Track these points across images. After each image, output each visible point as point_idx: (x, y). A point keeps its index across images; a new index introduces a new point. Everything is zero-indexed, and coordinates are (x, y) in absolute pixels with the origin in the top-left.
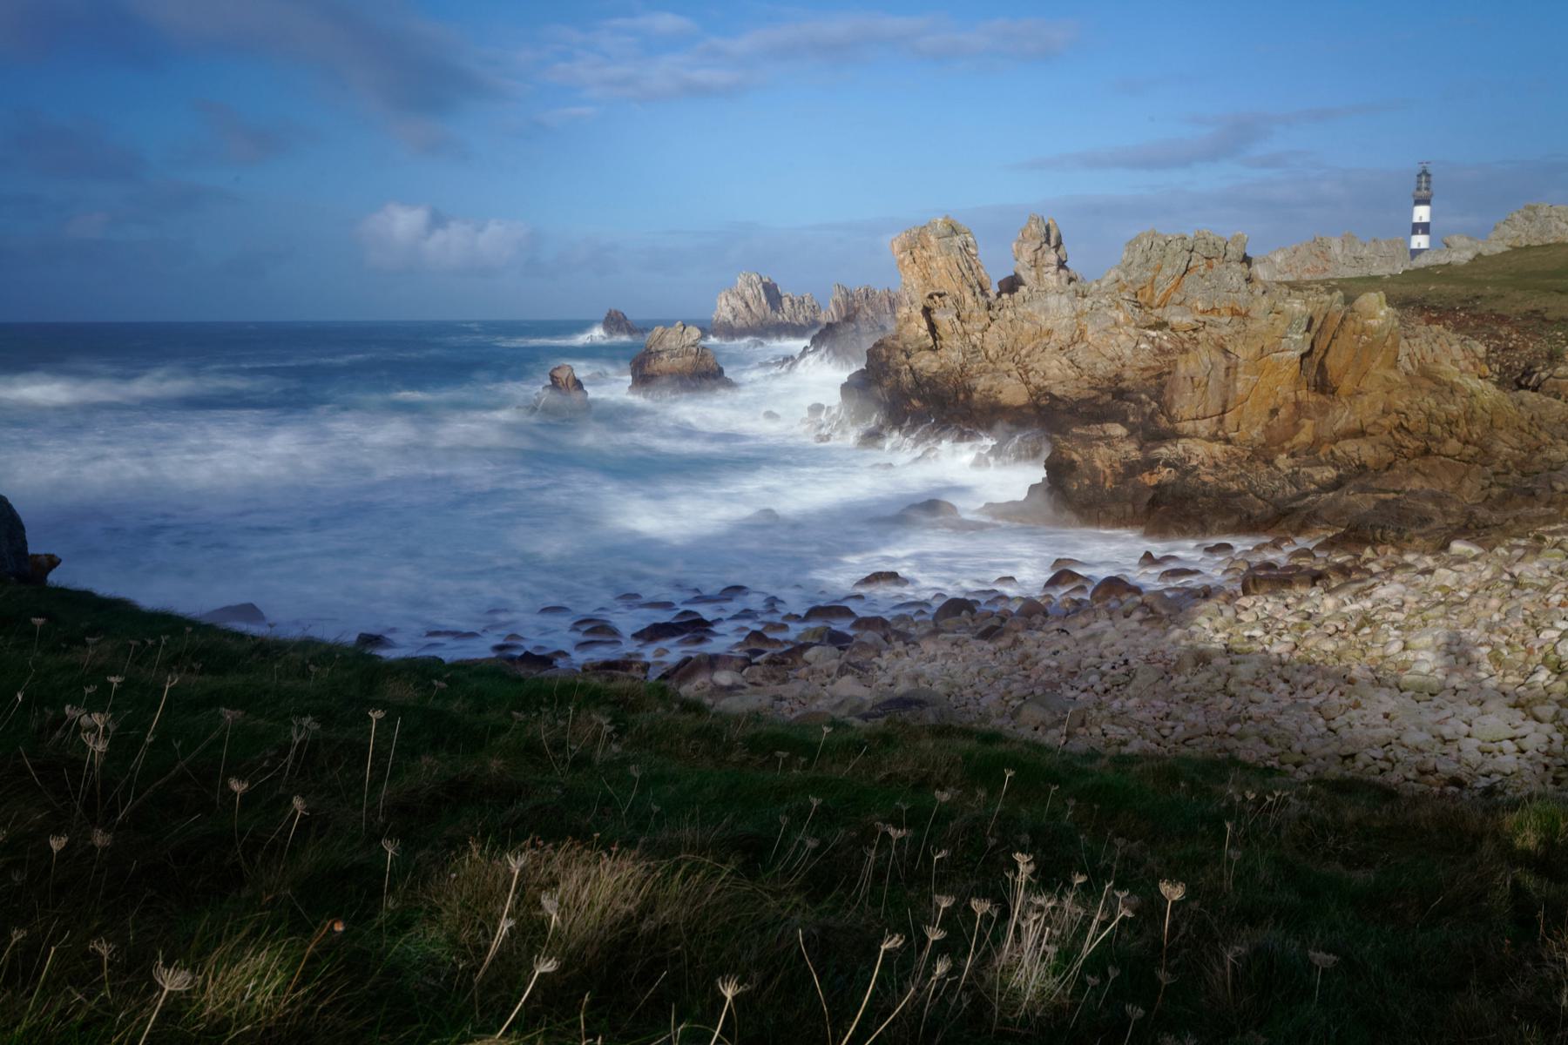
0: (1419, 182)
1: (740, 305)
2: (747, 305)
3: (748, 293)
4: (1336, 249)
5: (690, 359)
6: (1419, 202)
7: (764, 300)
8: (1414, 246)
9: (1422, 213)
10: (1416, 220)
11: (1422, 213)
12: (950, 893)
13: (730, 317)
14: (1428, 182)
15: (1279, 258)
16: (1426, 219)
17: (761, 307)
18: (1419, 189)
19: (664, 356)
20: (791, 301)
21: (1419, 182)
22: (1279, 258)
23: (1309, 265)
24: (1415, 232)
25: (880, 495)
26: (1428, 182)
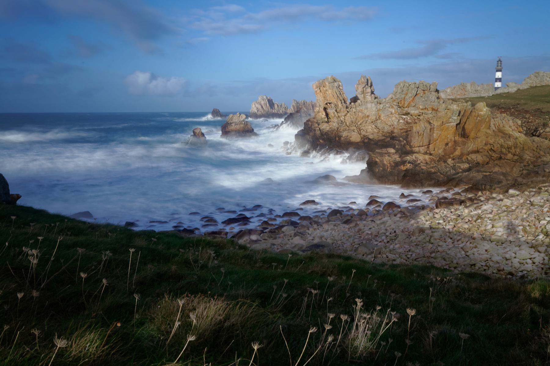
1: (260, 107)
2: (262, 107)
3: (262, 102)
4: (469, 87)
5: (242, 126)
7: (268, 105)
8: (496, 86)
9: (499, 75)
10: (497, 77)
11: (499, 75)
13: (256, 111)
15: (448, 90)
16: (500, 77)
17: (267, 108)
18: (498, 66)
21: (498, 64)
22: (448, 90)
23: (459, 93)
24: (496, 81)
26: (501, 64)
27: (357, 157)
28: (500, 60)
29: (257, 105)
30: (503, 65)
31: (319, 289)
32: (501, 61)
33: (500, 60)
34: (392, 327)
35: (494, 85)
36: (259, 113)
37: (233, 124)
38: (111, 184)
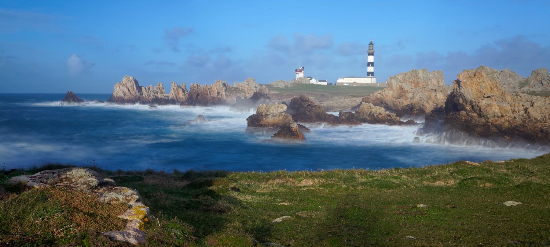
0: (370, 47)
1: (126, 90)
2: (129, 90)
3: (129, 85)
4: (421, 74)
5: (281, 118)
6: (369, 54)
7: (135, 88)
8: (369, 71)
9: (371, 59)
10: (369, 61)
11: (371, 59)
12: (346, 185)
13: (122, 95)
14: (372, 47)
15: (400, 77)
16: (372, 61)
17: (134, 91)
18: (369, 49)
19: (270, 116)
20: (145, 88)
21: (370, 47)
22: (400, 77)
23: (411, 80)
24: (368, 66)
25: (366, 145)
26: (372, 47)
27: (446, 137)
28: (371, 43)
31: (119, 219)
33: (371, 43)
35: (367, 69)
37: (270, 116)
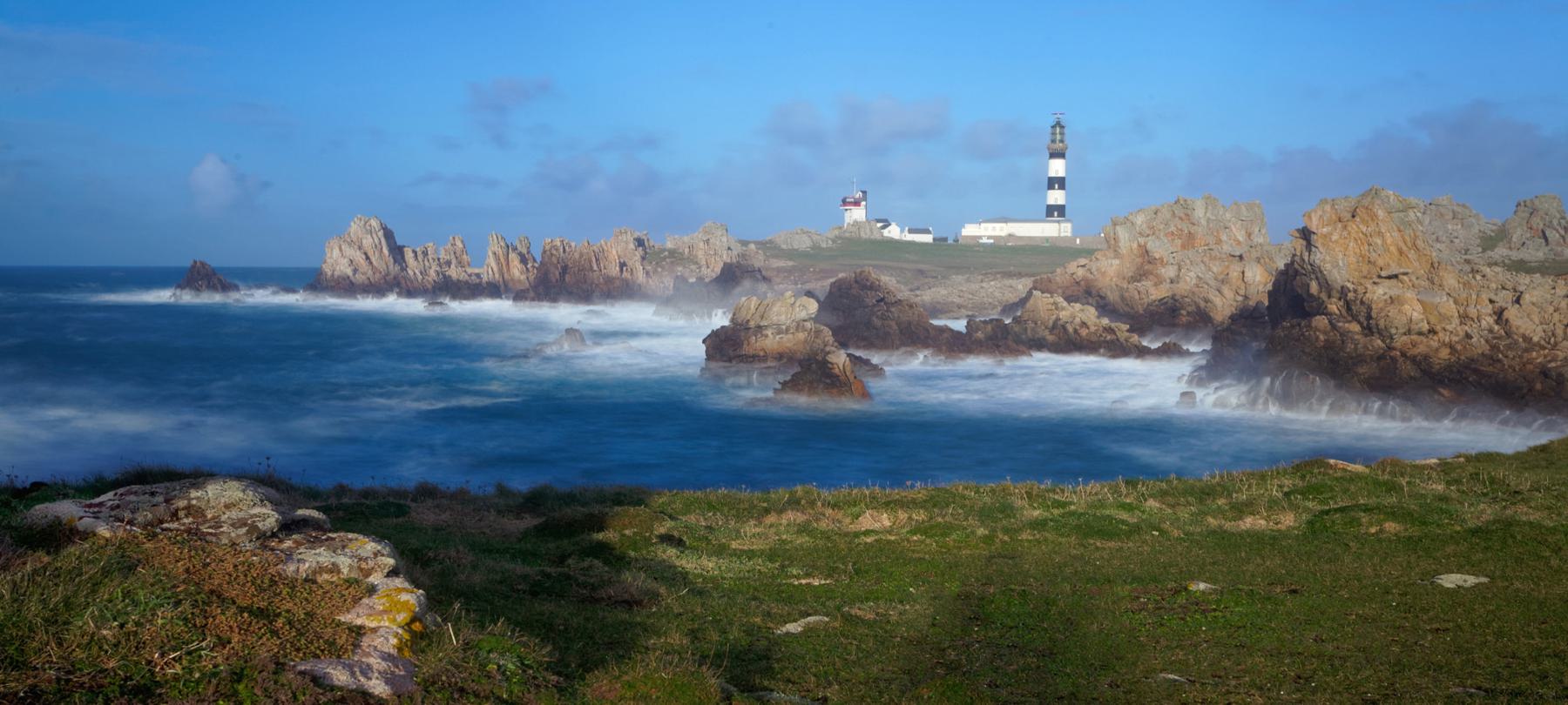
1: (359, 257)
2: (368, 258)
3: (367, 242)
4: (1199, 213)
5: (801, 336)
7: (386, 251)
8: (1051, 201)
9: (1057, 168)
10: (1052, 174)
11: (1057, 168)
13: (349, 272)
15: (1140, 220)
16: (1061, 174)
17: (383, 261)
18: (1053, 141)
21: (1054, 134)
23: (1173, 229)
24: (1051, 187)
26: (1062, 134)
28: (1058, 124)
29: (349, 251)
30: (1067, 138)
32: (1062, 127)
33: (1058, 124)
34: (1351, 480)
35: (1045, 197)
36: (360, 278)
37: (769, 332)
38: (914, 501)
